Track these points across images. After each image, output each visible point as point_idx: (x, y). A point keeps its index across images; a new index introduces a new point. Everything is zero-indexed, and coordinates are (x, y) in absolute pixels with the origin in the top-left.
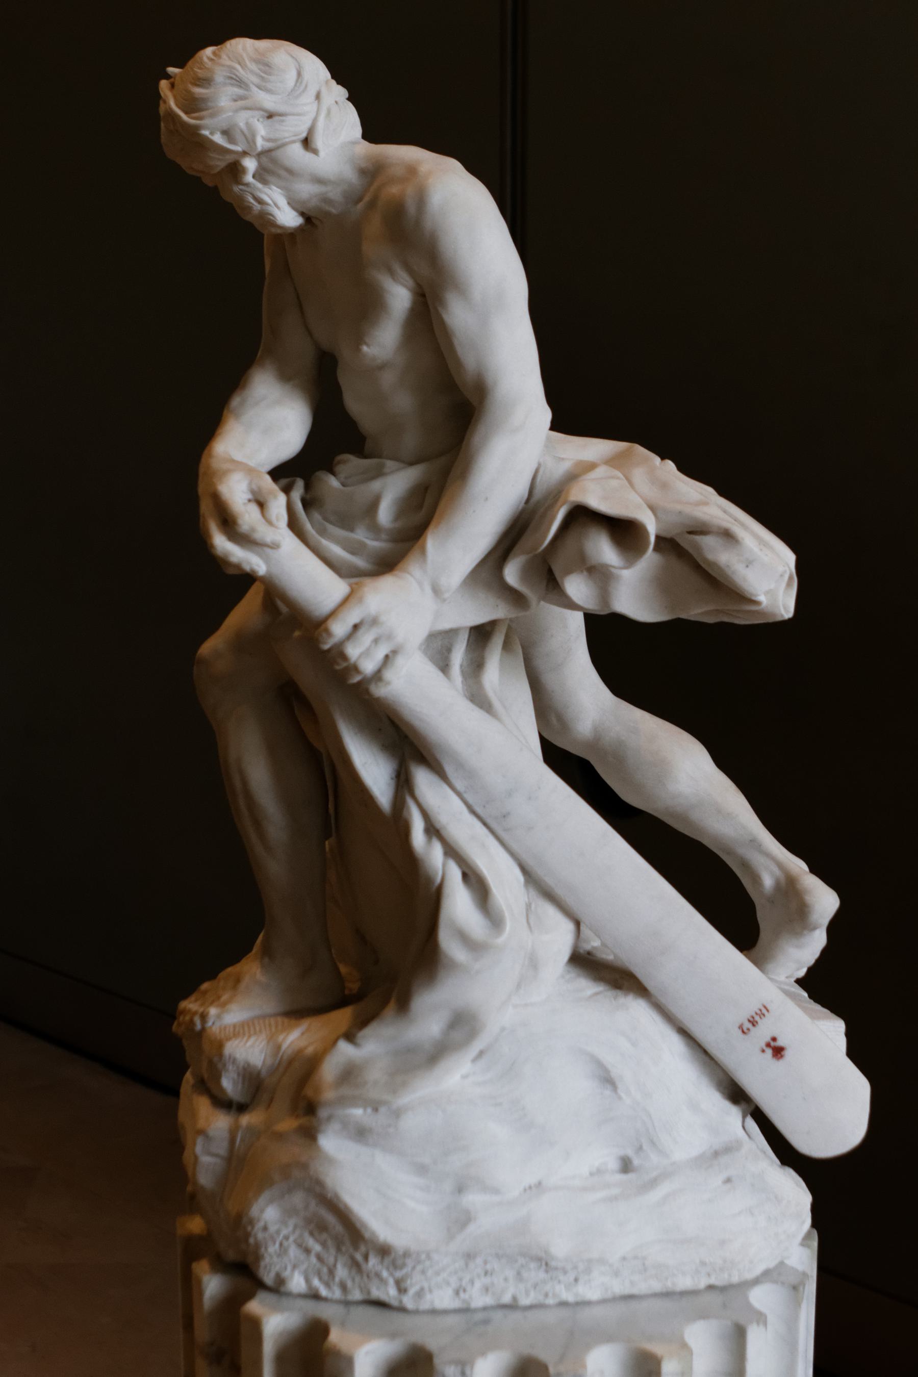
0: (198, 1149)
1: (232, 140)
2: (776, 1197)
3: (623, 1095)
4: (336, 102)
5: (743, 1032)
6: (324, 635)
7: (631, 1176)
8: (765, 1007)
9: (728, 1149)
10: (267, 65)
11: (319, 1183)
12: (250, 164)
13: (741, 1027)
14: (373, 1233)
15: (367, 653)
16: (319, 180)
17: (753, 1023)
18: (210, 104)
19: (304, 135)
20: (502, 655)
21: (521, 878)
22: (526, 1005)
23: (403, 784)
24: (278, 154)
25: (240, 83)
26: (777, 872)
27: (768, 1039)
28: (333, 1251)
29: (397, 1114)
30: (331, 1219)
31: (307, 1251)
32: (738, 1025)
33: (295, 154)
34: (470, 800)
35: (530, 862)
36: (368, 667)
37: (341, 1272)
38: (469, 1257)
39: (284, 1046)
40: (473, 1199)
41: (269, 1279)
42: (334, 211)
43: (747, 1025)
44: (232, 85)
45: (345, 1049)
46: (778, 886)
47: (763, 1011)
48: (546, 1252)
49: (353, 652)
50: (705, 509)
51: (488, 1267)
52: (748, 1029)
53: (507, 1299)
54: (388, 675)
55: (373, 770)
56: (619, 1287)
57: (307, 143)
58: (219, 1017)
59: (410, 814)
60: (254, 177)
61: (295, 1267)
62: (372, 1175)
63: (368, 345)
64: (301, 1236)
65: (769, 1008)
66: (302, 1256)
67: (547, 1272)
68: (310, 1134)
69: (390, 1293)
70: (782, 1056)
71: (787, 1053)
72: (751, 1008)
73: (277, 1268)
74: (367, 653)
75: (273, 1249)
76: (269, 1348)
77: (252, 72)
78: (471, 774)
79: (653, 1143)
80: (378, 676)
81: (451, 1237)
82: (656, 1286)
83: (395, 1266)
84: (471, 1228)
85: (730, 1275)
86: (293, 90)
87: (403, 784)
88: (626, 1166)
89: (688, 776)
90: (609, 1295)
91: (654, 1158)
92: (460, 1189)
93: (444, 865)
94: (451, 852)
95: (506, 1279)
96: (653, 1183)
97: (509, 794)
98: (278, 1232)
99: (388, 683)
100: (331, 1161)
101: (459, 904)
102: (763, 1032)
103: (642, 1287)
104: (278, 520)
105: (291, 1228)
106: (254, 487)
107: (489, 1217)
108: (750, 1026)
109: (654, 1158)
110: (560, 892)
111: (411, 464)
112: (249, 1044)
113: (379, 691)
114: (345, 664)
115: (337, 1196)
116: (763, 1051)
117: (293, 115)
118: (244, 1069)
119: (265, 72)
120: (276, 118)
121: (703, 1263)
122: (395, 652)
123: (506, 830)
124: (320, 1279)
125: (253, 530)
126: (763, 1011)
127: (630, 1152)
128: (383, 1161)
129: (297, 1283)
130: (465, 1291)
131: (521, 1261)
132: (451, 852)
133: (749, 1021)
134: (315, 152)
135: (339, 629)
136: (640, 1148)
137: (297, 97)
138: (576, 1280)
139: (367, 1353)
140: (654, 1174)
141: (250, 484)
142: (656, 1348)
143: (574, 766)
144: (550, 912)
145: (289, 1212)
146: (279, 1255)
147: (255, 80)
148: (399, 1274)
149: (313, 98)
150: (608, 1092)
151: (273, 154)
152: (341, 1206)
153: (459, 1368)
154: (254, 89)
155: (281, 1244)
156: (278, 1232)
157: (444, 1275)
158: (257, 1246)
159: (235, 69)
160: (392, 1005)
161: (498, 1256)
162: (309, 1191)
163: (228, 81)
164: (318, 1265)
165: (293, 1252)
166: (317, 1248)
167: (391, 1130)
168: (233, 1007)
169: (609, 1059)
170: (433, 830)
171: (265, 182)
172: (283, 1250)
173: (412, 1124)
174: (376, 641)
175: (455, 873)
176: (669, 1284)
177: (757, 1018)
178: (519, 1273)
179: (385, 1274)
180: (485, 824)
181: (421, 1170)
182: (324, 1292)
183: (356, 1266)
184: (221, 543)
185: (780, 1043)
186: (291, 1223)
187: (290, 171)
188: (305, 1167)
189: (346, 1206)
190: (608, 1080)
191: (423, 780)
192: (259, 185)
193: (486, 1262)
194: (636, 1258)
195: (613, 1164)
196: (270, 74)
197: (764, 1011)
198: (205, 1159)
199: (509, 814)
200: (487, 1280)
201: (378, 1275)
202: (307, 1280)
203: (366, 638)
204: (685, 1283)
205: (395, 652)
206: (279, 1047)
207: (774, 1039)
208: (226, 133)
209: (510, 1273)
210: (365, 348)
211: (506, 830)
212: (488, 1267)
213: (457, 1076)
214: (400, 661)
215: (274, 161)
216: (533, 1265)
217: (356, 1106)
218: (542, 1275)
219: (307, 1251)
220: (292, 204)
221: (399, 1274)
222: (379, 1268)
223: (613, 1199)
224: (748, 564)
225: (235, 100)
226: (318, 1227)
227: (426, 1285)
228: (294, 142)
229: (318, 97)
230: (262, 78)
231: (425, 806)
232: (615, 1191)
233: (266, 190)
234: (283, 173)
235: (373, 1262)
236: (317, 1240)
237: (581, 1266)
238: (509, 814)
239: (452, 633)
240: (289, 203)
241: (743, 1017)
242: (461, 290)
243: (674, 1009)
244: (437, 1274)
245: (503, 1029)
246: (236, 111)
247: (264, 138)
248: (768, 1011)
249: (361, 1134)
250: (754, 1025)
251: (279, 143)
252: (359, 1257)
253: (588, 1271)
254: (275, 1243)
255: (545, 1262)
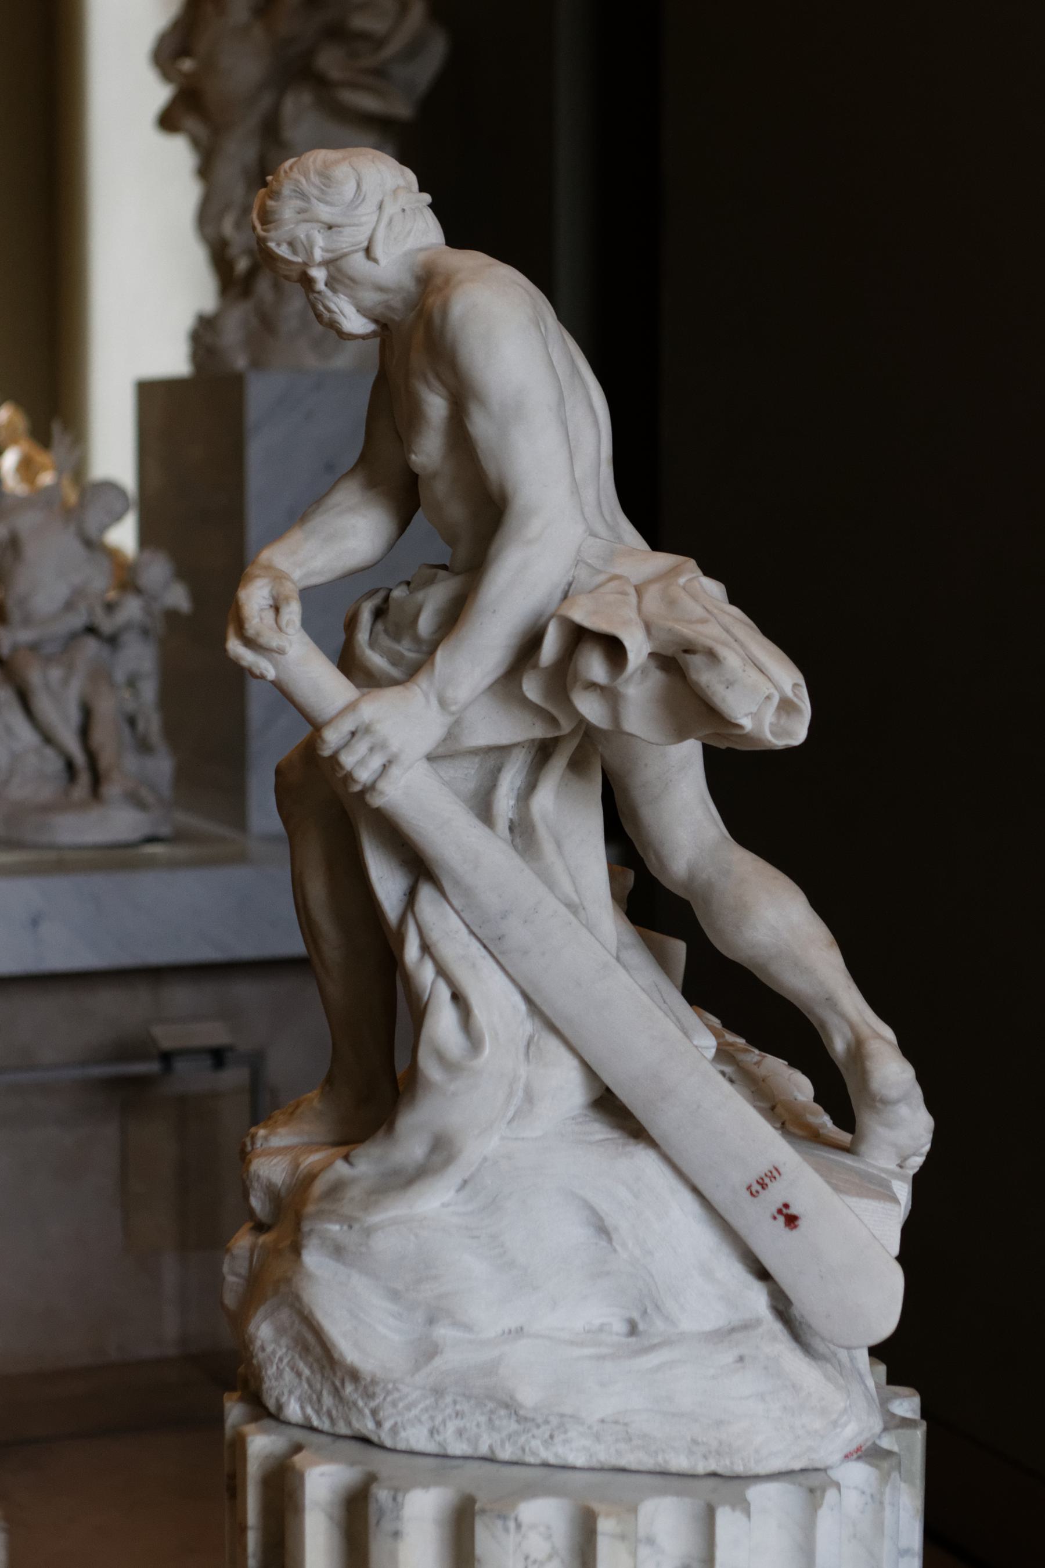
0: (225, 1269)
1: (295, 252)
2: (794, 1386)
3: (618, 1248)
4: (404, 210)
5: (752, 1194)
6: (319, 741)
7: (633, 1340)
8: (776, 1169)
9: (748, 1326)
10: (328, 178)
11: (298, 1298)
12: (319, 275)
13: (749, 1188)
14: (341, 1354)
15: (362, 762)
16: (380, 289)
17: (763, 1186)
18: (277, 217)
19: (365, 244)
20: (563, 776)
21: (522, 1007)
22: (516, 1139)
23: (411, 897)
24: (343, 263)
25: (303, 196)
26: (849, 1035)
27: (780, 1205)
28: (319, 1377)
29: (368, 1232)
30: (310, 1338)
31: (299, 1374)
32: (745, 1186)
33: (358, 263)
34: (467, 921)
35: (529, 991)
36: (364, 776)
37: (328, 1400)
38: (438, 1392)
39: (302, 1167)
40: (443, 1332)
41: (271, 1404)
42: (396, 318)
43: (756, 1187)
44: (297, 197)
45: (341, 1168)
46: (848, 1049)
47: (774, 1174)
48: (512, 1397)
49: (348, 760)
50: (700, 628)
51: (458, 1407)
52: (757, 1192)
53: (483, 1449)
54: (381, 785)
55: (387, 882)
56: (605, 1454)
57: (368, 251)
58: (266, 1138)
59: (406, 929)
60: (326, 285)
61: (291, 1392)
62: (351, 1299)
63: (416, 454)
64: (293, 1358)
65: (781, 1170)
66: (296, 1381)
67: (518, 1422)
68: (297, 1249)
69: (367, 1426)
70: (796, 1227)
71: (802, 1223)
72: (761, 1168)
73: (275, 1393)
74: (362, 762)
75: (271, 1371)
76: (253, 1469)
77: (314, 185)
78: (467, 892)
79: (657, 1307)
80: (371, 787)
81: (417, 1368)
82: (648, 1462)
83: (371, 1396)
84: (437, 1361)
85: (732, 1463)
86: (352, 201)
87: (411, 897)
88: (633, 1329)
89: (780, 926)
90: (594, 1463)
91: (660, 1325)
92: (431, 1321)
93: (433, 983)
94: (442, 972)
95: (478, 1425)
96: (652, 1348)
97: (504, 916)
98: (274, 1352)
99: (381, 793)
100: (310, 1276)
101: (443, 1023)
102: (776, 1195)
103: (630, 1459)
104: (287, 625)
105: (284, 1350)
106: (274, 593)
107: (456, 1356)
108: (759, 1188)
109: (660, 1325)
110: (558, 1024)
111: (457, 574)
112: (275, 1161)
113: (376, 801)
114: (344, 772)
115: (311, 1312)
116: (775, 1218)
117: (350, 226)
118: (268, 1187)
119: (324, 185)
120: (334, 229)
121: (694, 1441)
122: (390, 762)
123: (502, 953)
124: (313, 1408)
125: (258, 634)
126: (774, 1174)
127: (636, 1315)
128: (359, 1283)
129: (293, 1410)
130: (438, 1432)
131: (491, 1405)
132: (442, 972)
133: (758, 1182)
134: (375, 261)
135: (332, 737)
136: (645, 1312)
137: (356, 207)
138: (552, 1437)
139: (322, 1475)
140: (656, 1341)
141: (271, 591)
142: (596, 1506)
143: (652, 903)
144: (553, 1046)
145: (280, 1331)
146: (276, 1379)
147: (315, 192)
148: (373, 1404)
149: (375, 208)
150: (603, 1243)
151: (338, 262)
152: (315, 1323)
153: (392, 1493)
154: (314, 201)
155: (278, 1368)
156: (274, 1352)
157: (415, 1412)
158: (260, 1368)
159: (299, 181)
160: (384, 1127)
161: (468, 1397)
162: (292, 1306)
163: (294, 194)
164: (309, 1391)
165: (288, 1376)
166: (307, 1372)
167: (363, 1249)
168: (282, 1131)
169: (604, 1207)
170: (426, 948)
171: (334, 291)
172: (280, 1373)
173: (386, 1244)
174: (371, 749)
175: (444, 993)
176: (660, 1459)
177: (767, 1180)
178: (490, 1420)
179: (361, 1403)
180: (485, 947)
181: (395, 1295)
182: (316, 1423)
183: (337, 1393)
184: (235, 647)
185: (793, 1211)
186: (284, 1341)
187: (353, 280)
188: (288, 1281)
189: (318, 1324)
190: (603, 1230)
191: (426, 893)
192: (329, 293)
193: (455, 1402)
194: (616, 1422)
195: (620, 1327)
196: (329, 187)
197: (775, 1174)
198: (231, 1279)
199: (503, 936)
200: (460, 1423)
201: (355, 1404)
202: (302, 1408)
203: (361, 747)
204: (680, 1462)
205: (390, 762)
206: (298, 1166)
207: (786, 1206)
208: (291, 244)
209: (483, 1419)
210: (413, 457)
211: (502, 953)
212: (458, 1407)
213: (435, 1201)
214: (395, 771)
215: (339, 270)
216: (503, 1412)
217: (330, 1221)
218: (514, 1426)
219: (299, 1374)
220: (362, 310)
221: (373, 1404)
222: (355, 1396)
223: (601, 1358)
224: (729, 685)
225: (299, 213)
226: (305, 1349)
227: (399, 1419)
228: (356, 251)
229: (380, 207)
230: (322, 190)
231: (421, 923)
232: (604, 1350)
233: (335, 299)
234: (347, 281)
235: (349, 1389)
236: (306, 1363)
237: (554, 1421)
238: (503, 936)
239: (502, 751)
240: (358, 311)
241: (751, 1177)
242: (482, 402)
243: (676, 1160)
244: (408, 1408)
245: (485, 1159)
246: (298, 223)
247: (323, 250)
248: (779, 1174)
249: (338, 1251)
250: (763, 1188)
251: (339, 253)
252: (338, 1383)
253: (562, 1427)
254: (272, 1363)
255: (511, 1406)
